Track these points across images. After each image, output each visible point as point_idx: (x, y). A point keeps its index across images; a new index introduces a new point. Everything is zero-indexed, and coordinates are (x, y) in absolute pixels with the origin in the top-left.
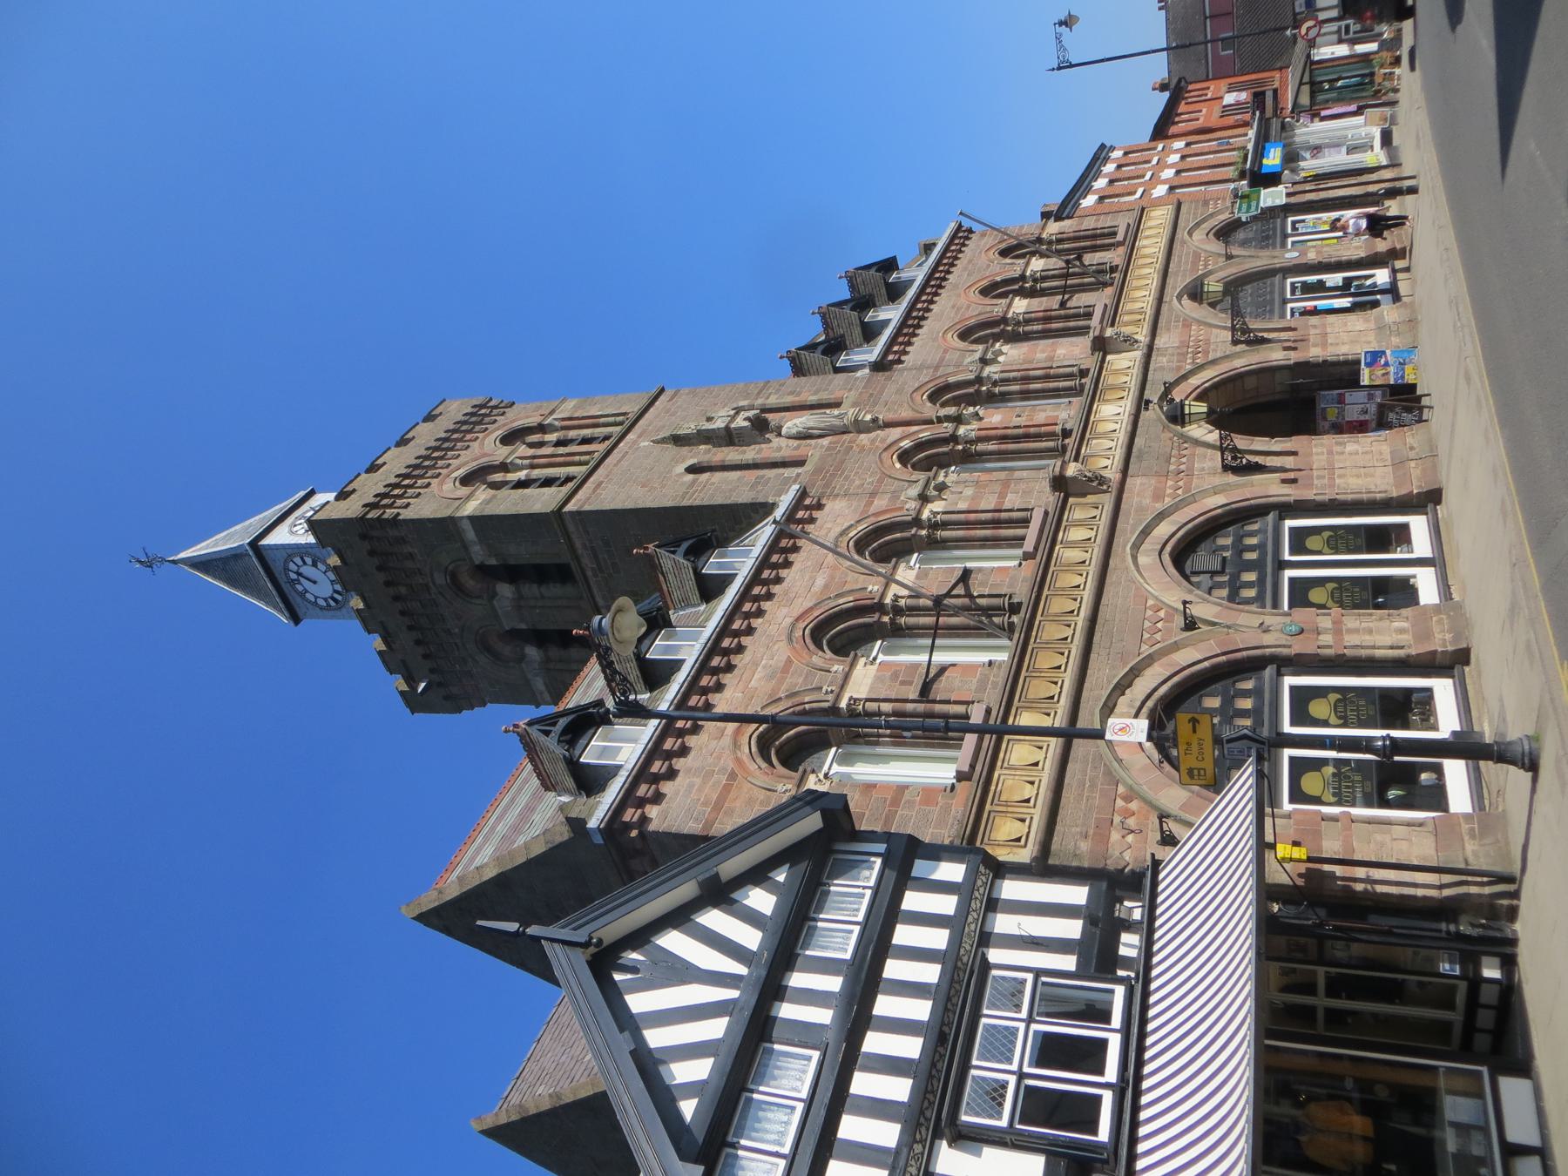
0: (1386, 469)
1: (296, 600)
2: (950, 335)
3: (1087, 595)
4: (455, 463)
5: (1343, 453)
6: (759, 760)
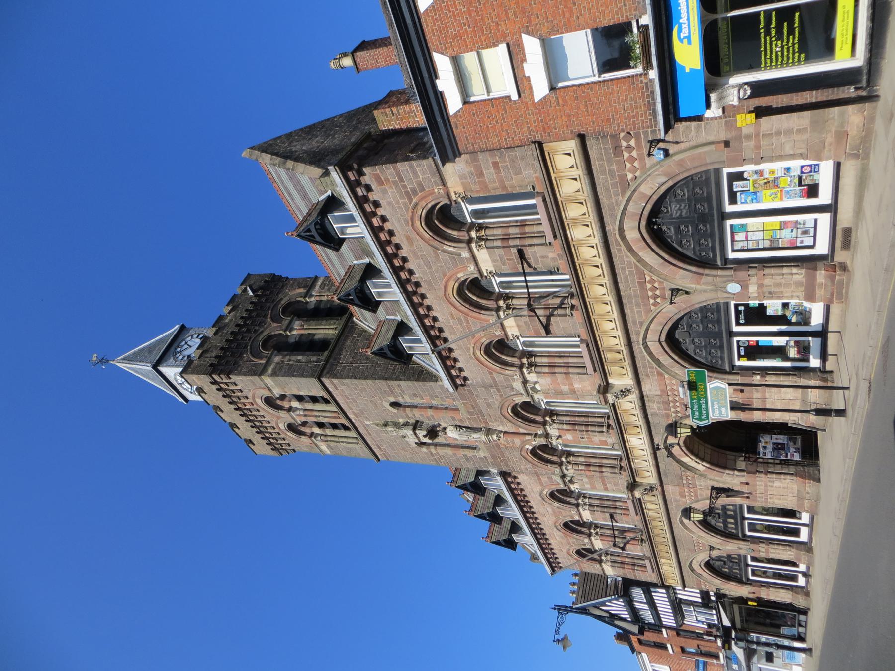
5: (772, 486)
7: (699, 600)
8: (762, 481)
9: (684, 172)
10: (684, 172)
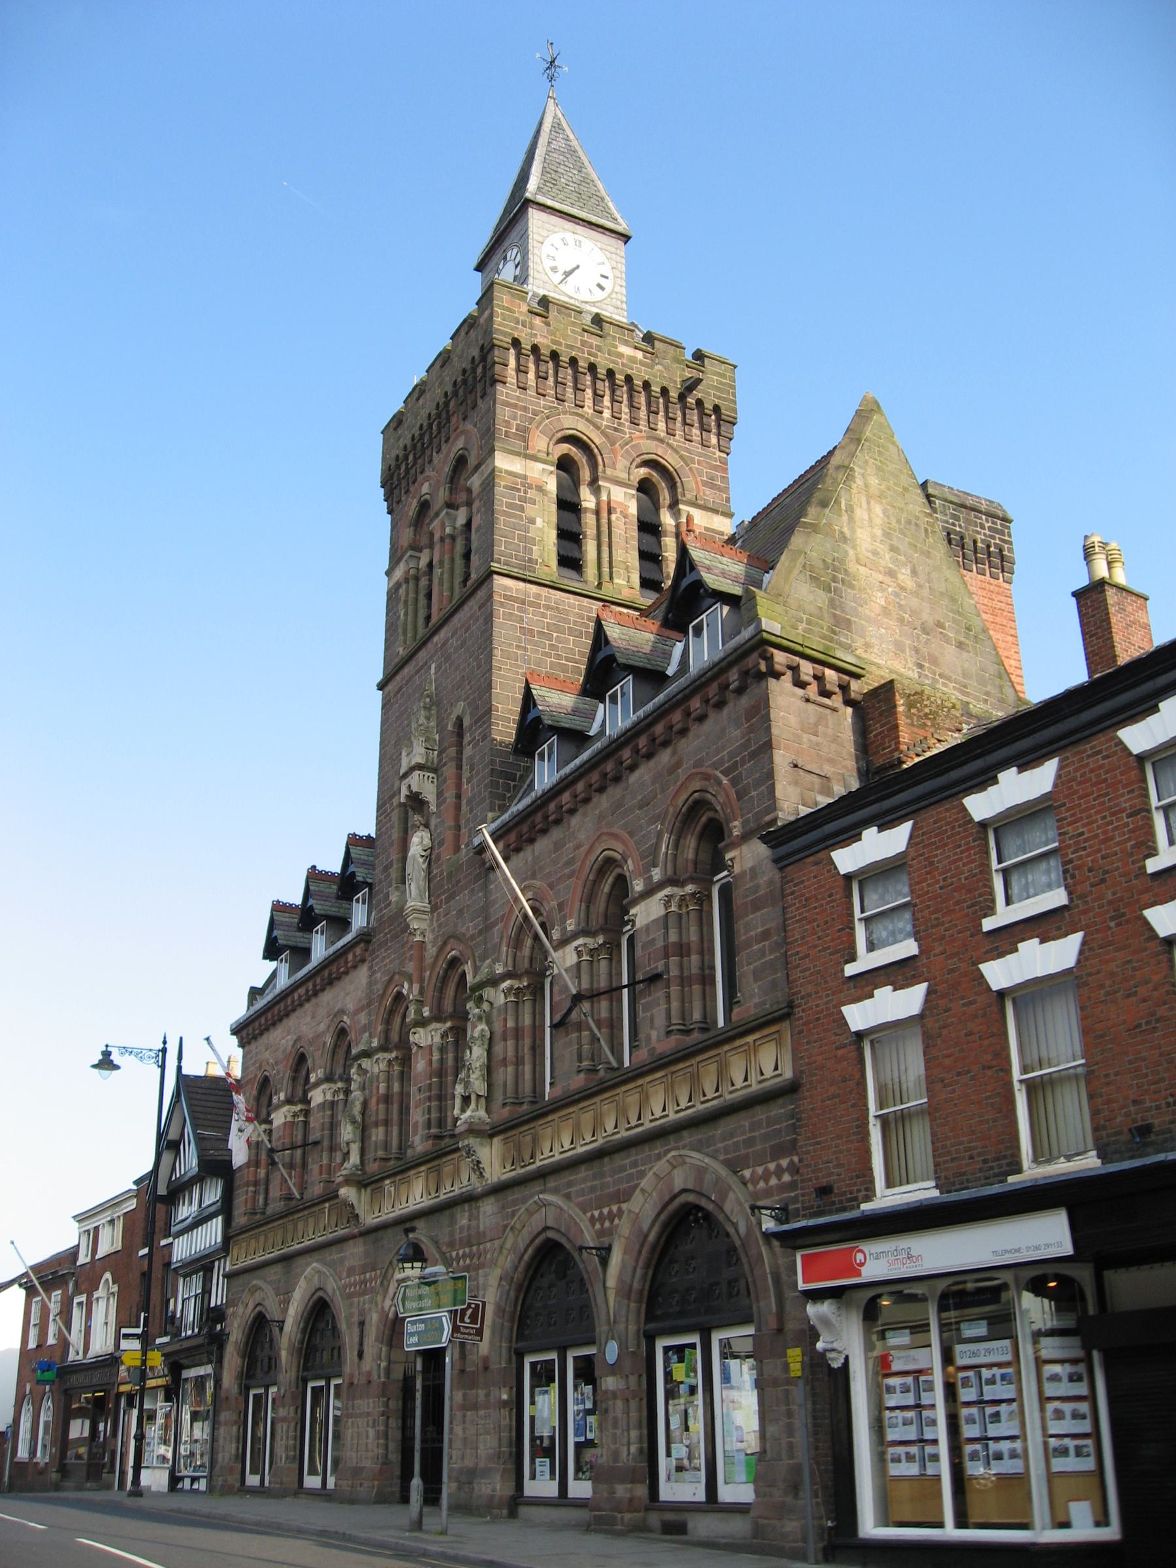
7: (213, 1304)
8: (374, 1407)
9: (750, 1265)
10: (750, 1265)
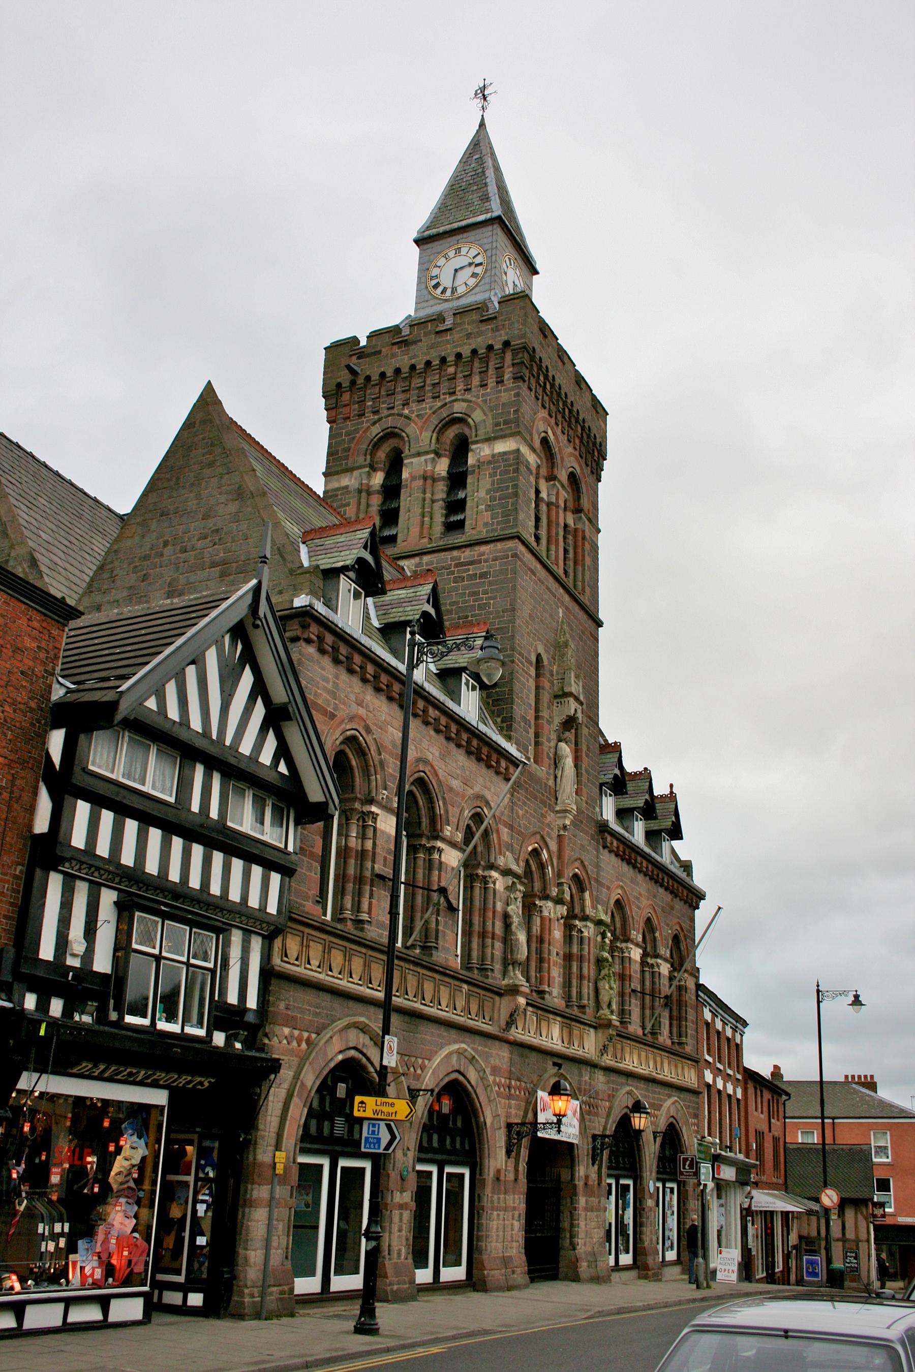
0: (500, 1251)
1: (436, 246)
2: (620, 892)
3: (433, 1011)
4: (559, 431)
6: (341, 738)
